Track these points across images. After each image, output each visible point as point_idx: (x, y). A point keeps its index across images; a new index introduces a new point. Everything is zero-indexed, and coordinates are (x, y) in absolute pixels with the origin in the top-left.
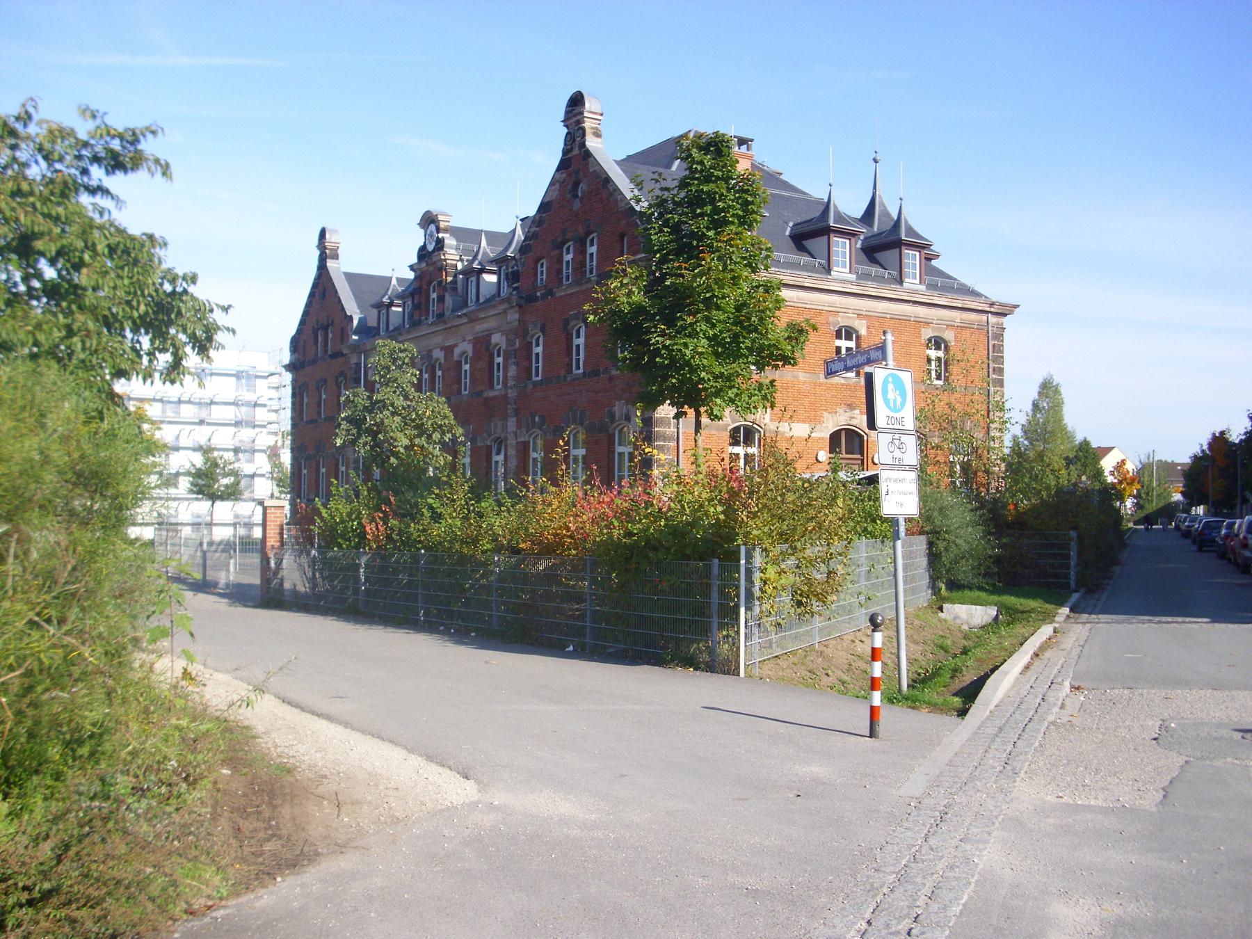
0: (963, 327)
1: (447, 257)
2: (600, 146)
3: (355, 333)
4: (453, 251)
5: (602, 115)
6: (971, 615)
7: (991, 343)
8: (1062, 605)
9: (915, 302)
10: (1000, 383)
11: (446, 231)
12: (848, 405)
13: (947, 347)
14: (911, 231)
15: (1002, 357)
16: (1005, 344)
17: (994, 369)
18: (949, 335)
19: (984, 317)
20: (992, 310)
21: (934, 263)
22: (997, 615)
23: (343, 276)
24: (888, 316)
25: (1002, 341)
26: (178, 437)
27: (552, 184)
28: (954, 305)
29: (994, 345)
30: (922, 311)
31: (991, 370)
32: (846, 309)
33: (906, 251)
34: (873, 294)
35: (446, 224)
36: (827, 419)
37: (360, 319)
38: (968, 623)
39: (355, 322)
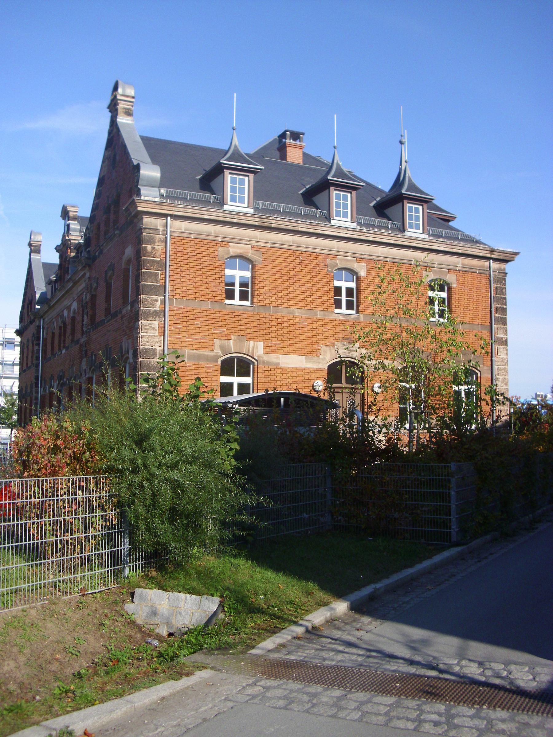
0: (464, 271)
1: (71, 237)
2: (130, 122)
3: (38, 303)
4: (78, 234)
5: (133, 97)
6: (176, 610)
7: (493, 286)
8: (340, 595)
9: (415, 248)
10: (504, 322)
11: (74, 218)
12: (347, 339)
13: (449, 289)
14: (413, 187)
15: (505, 299)
16: (508, 287)
17: (497, 309)
18: (451, 278)
19: (486, 263)
20: (493, 256)
21: (451, 224)
22: (215, 614)
23: (41, 265)
24: (388, 260)
25: (505, 284)
26: (12, 388)
27: (103, 162)
28: (454, 251)
29: (496, 288)
30: (421, 255)
31: (493, 309)
32: (344, 253)
33: (407, 205)
34: (371, 239)
35: (75, 214)
36: (325, 352)
37: (42, 294)
38: (168, 624)
39: (38, 296)
